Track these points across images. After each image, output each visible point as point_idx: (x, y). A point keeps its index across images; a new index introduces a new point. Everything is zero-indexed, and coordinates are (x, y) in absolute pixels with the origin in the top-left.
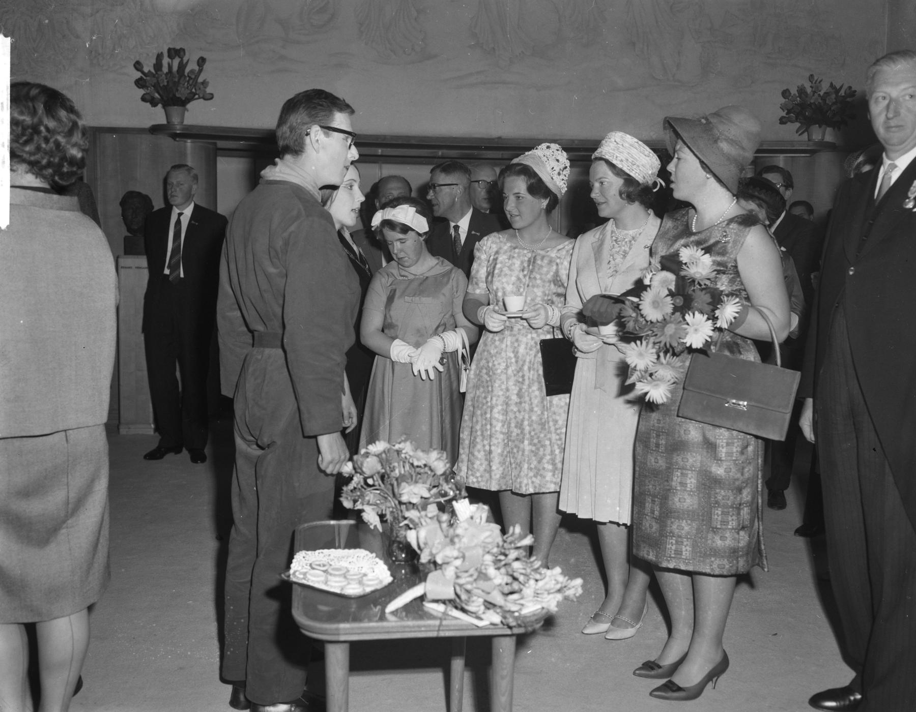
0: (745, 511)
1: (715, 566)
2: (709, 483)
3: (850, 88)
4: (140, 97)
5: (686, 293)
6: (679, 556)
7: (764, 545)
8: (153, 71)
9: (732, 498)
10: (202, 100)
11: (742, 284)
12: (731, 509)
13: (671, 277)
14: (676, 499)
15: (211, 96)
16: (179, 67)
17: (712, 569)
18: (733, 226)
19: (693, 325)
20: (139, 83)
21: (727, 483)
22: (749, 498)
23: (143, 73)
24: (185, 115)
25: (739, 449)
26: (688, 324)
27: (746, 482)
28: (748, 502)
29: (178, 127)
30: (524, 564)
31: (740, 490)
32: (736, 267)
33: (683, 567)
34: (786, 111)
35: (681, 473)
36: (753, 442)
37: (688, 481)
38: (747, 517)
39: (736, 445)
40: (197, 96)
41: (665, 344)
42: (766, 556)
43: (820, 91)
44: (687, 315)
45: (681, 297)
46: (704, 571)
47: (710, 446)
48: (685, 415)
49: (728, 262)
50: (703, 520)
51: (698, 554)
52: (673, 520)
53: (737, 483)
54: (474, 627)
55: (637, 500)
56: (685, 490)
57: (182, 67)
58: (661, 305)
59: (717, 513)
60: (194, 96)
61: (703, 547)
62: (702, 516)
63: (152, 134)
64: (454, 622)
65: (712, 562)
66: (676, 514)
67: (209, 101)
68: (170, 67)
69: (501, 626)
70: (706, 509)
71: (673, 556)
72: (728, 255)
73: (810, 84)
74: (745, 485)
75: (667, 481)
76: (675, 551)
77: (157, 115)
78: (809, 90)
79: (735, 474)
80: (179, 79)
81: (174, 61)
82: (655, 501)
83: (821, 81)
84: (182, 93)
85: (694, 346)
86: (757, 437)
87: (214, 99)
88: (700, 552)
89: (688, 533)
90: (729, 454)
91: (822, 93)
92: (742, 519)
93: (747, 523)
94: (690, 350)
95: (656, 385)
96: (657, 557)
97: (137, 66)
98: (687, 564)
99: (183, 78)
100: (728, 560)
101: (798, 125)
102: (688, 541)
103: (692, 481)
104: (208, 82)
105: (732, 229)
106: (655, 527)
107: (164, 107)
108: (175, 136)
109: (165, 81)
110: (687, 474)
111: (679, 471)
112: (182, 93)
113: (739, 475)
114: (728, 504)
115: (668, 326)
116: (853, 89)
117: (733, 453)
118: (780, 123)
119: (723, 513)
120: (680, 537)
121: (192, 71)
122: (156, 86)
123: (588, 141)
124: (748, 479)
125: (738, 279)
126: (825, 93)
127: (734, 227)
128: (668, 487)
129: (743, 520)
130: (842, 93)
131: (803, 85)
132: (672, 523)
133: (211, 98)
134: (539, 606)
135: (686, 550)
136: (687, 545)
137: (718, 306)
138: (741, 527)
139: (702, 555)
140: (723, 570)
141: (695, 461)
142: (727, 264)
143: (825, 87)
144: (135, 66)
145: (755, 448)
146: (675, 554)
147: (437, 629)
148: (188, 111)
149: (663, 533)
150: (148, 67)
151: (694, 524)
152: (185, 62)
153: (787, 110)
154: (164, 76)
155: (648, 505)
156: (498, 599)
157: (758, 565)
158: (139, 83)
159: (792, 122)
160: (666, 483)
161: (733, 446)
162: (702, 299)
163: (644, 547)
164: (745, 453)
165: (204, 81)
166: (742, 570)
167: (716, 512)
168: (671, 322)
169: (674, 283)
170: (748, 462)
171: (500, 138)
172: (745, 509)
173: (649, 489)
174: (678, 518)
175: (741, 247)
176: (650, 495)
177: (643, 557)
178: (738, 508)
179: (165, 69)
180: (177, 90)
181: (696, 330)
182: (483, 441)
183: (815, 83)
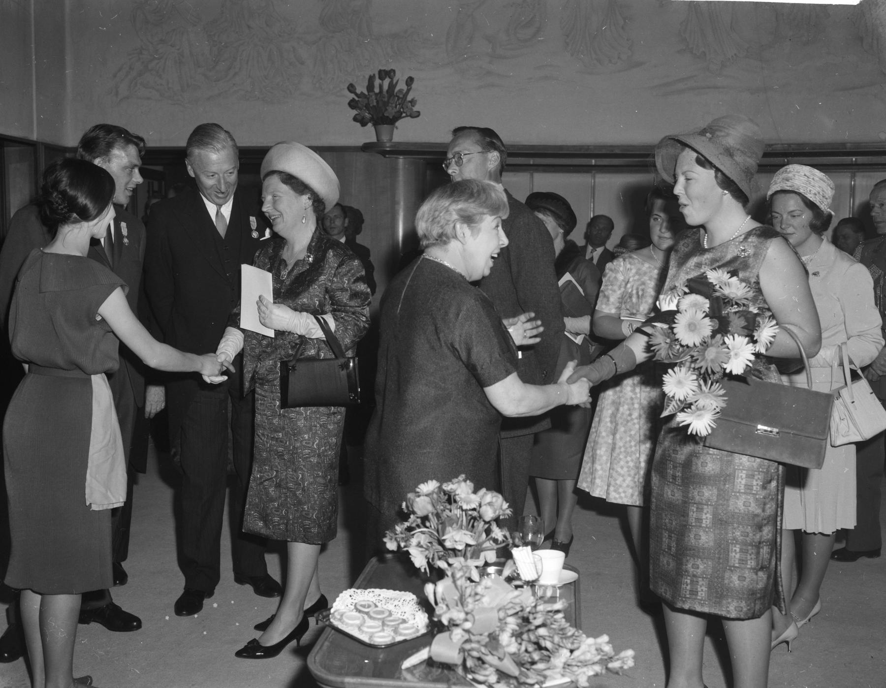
0: (765, 550)
1: (732, 608)
2: (720, 522)
6: (694, 597)
8: (366, 93)
10: (409, 118)
11: (765, 301)
12: (750, 547)
14: (692, 536)
15: (417, 114)
17: (728, 612)
18: (752, 239)
24: (394, 133)
28: (768, 540)
29: (388, 145)
31: (759, 527)
32: (758, 283)
33: (699, 609)
35: (697, 508)
37: (704, 517)
38: (766, 556)
39: (756, 477)
40: (404, 115)
41: (707, 369)
49: (750, 278)
53: (756, 520)
57: (392, 86)
58: (698, 327)
59: (735, 550)
60: (402, 114)
61: (719, 587)
63: (364, 151)
65: (729, 603)
66: (692, 552)
67: (415, 119)
68: (381, 86)
70: (722, 546)
72: (749, 270)
75: (683, 516)
77: (367, 134)
79: (754, 508)
80: (389, 99)
81: (384, 81)
82: (671, 537)
84: (390, 112)
85: (734, 373)
87: (420, 117)
88: (717, 592)
89: (704, 572)
90: (749, 487)
92: (761, 558)
94: (730, 376)
95: (699, 416)
98: (702, 605)
99: (392, 98)
100: (746, 602)
103: (707, 517)
105: (752, 242)
106: (672, 564)
108: (384, 153)
109: (375, 101)
111: (695, 505)
112: (390, 112)
113: (759, 511)
115: (708, 349)
117: (752, 486)
120: (694, 576)
121: (400, 91)
124: (770, 516)
125: (761, 298)
127: (753, 240)
128: (684, 523)
129: (763, 559)
132: (687, 561)
133: (418, 116)
135: (702, 590)
136: (703, 584)
138: (759, 567)
142: (750, 279)
144: (348, 88)
146: (690, 594)
148: (397, 128)
149: (680, 572)
150: (361, 89)
151: (710, 563)
152: (395, 82)
155: (665, 540)
158: (352, 104)
160: (682, 518)
162: (737, 323)
163: (662, 585)
165: (413, 99)
167: (734, 549)
168: (712, 345)
172: (765, 548)
173: (666, 523)
174: (694, 556)
175: (763, 260)
176: (666, 530)
177: (661, 594)
179: (377, 90)
180: (386, 110)
181: (736, 354)
182: (626, 457)
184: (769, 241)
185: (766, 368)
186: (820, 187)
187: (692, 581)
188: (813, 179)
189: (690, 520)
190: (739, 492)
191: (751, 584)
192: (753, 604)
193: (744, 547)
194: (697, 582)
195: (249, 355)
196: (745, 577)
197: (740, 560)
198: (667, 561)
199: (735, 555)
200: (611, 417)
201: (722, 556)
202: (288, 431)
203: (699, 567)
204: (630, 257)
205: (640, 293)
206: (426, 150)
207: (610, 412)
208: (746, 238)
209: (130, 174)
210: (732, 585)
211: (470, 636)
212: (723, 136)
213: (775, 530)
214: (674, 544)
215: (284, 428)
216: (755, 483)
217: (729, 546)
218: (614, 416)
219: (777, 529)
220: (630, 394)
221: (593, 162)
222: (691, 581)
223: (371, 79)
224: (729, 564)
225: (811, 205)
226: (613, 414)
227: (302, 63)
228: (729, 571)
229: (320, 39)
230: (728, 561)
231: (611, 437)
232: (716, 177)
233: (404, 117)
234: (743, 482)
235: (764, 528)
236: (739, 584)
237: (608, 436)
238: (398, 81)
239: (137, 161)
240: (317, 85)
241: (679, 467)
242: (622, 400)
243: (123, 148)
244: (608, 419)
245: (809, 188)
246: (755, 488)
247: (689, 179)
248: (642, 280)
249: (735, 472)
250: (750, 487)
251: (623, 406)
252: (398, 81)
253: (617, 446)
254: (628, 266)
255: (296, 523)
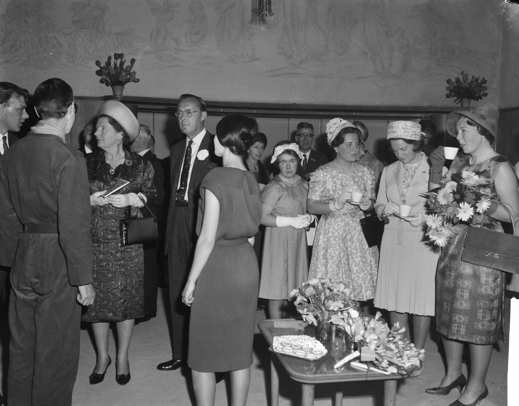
0: (495, 312)
3: (484, 79)
4: (99, 80)
5: (462, 193)
6: (458, 333)
7: (505, 329)
9: (488, 305)
10: (133, 82)
12: (487, 311)
13: (455, 184)
15: (137, 80)
16: (120, 65)
17: (476, 341)
19: (463, 209)
20: (98, 73)
21: (486, 296)
22: (497, 305)
23: (100, 67)
25: (492, 279)
26: (460, 208)
27: (496, 297)
28: (497, 307)
30: (404, 342)
31: (492, 301)
33: (461, 339)
34: (449, 91)
35: (461, 290)
36: (500, 276)
37: (465, 295)
38: (495, 315)
39: (490, 277)
40: (131, 80)
42: (506, 335)
43: (468, 80)
44: (461, 203)
45: (459, 195)
46: (472, 341)
47: (476, 276)
48: (465, 261)
50: (472, 315)
51: (469, 333)
52: (456, 314)
53: (491, 297)
54: (384, 375)
55: (438, 304)
56: (463, 299)
58: (447, 197)
59: (480, 312)
62: (472, 313)
64: (372, 373)
65: (477, 337)
66: (458, 311)
69: (398, 374)
71: (456, 333)
73: (462, 76)
74: (495, 298)
76: (457, 330)
78: (461, 80)
79: (490, 292)
81: (118, 60)
83: (468, 75)
85: (463, 220)
86: (502, 271)
87: (140, 82)
89: (464, 322)
91: (469, 82)
92: (493, 316)
93: (495, 318)
94: (461, 222)
96: (447, 333)
97: (97, 63)
98: (463, 337)
99: (122, 70)
100: (485, 337)
101: (455, 98)
102: (463, 326)
103: (466, 295)
104: (136, 73)
105: (493, 163)
106: (448, 317)
107: (111, 86)
109: (114, 72)
110: (464, 291)
111: (460, 289)
113: (492, 293)
114: (486, 308)
116: (485, 80)
117: (489, 281)
118: (446, 97)
119: (483, 312)
120: (459, 323)
121: (128, 67)
122: (108, 75)
123: (280, 104)
126: (470, 82)
128: (454, 297)
129: (494, 316)
130: (479, 81)
131: (458, 77)
132: (455, 316)
133: (138, 81)
134: (410, 364)
135: (463, 330)
136: (463, 328)
137: (478, 201)
139: (471, 333)
140: (483, 342)
141: (468, 284)
143: (470, 79)
144: (96, 63)
145: (501, 279)
147: (366, 376)
149: (451, 321)
153: (450, 90)
154: (113, 69)
155: (445, 306)
156: (395, 360)
157: (501, 339)
158: (98, 73)
159: (452, 97)
161: (489, 277)
162: (471, 196)
163: (443, 328)
164: (496, 281)
166: (492, 342)
169: (456, 187)
170: (497, 286)
171: (294, 104)
172: (495, 311)
174: (459, 313)
175: (497, 172)
176: (446, 301)
177: (442, 333)
178: (491, 310)
181: (465, 212)
183: (465, 76)
184: (501, 163)
185: (496, 223)
186: (412, 131)
187: (458, 326)
188: (407, 129)
189: (457, 296)
190: (482, 284)
191: (488, 328)
192: (489, 338)
193: (485, 311)
194: (461, 326)
195: (100, 216)
196: (485, 325)
197: (482, 317)
198: (446, 316)
199: (480, 314)
200: (323, 256)
201: (473, 314)
202: (127, 259)
203: (460, 319)
204: (325, 168)
205: (334, 189)
206: (139, 101)
207: (322, 253)
208: (490, 161)
209: (21, 114)
210: (478, 328)
211: (374, 344)
212: (479, 110)
213: (501, 302)
214: (449, 308)
215: (124, 258)
216: (490, 280)
217: (477, 310)
218: (325, 255)
219: (502, 301)
220: (334, 242)
221: (222, 110)
222: (457, 325)
223: (109, 58)
224: (477, 318)
225: (409, 142)
226: (324, 254)
227: (61, 46)
228: (477, 322)
229: (73, 32)
230: (476, 317)
231: (324, 267)
232: (478, 129)
233: (131, 82)
234: (484, 279)
235: (494, 301)
236: (481, 328)
237: (322, 267)
238: (125, 61)
239: (25, 105)
240: (71, 60)
241: (453, 270)
242: (329, 245)
243: (18, 98)
244: (321, 258)
245: (407, 134)
246: (490, 282)
247: (464, 131)
248: (334, 181)
249: (480, 274)
250: (487, 282)
251: (330, 249)
252: (125, 61)
253: (329, 271)
254: (325, 174)
255: (132, 308)
